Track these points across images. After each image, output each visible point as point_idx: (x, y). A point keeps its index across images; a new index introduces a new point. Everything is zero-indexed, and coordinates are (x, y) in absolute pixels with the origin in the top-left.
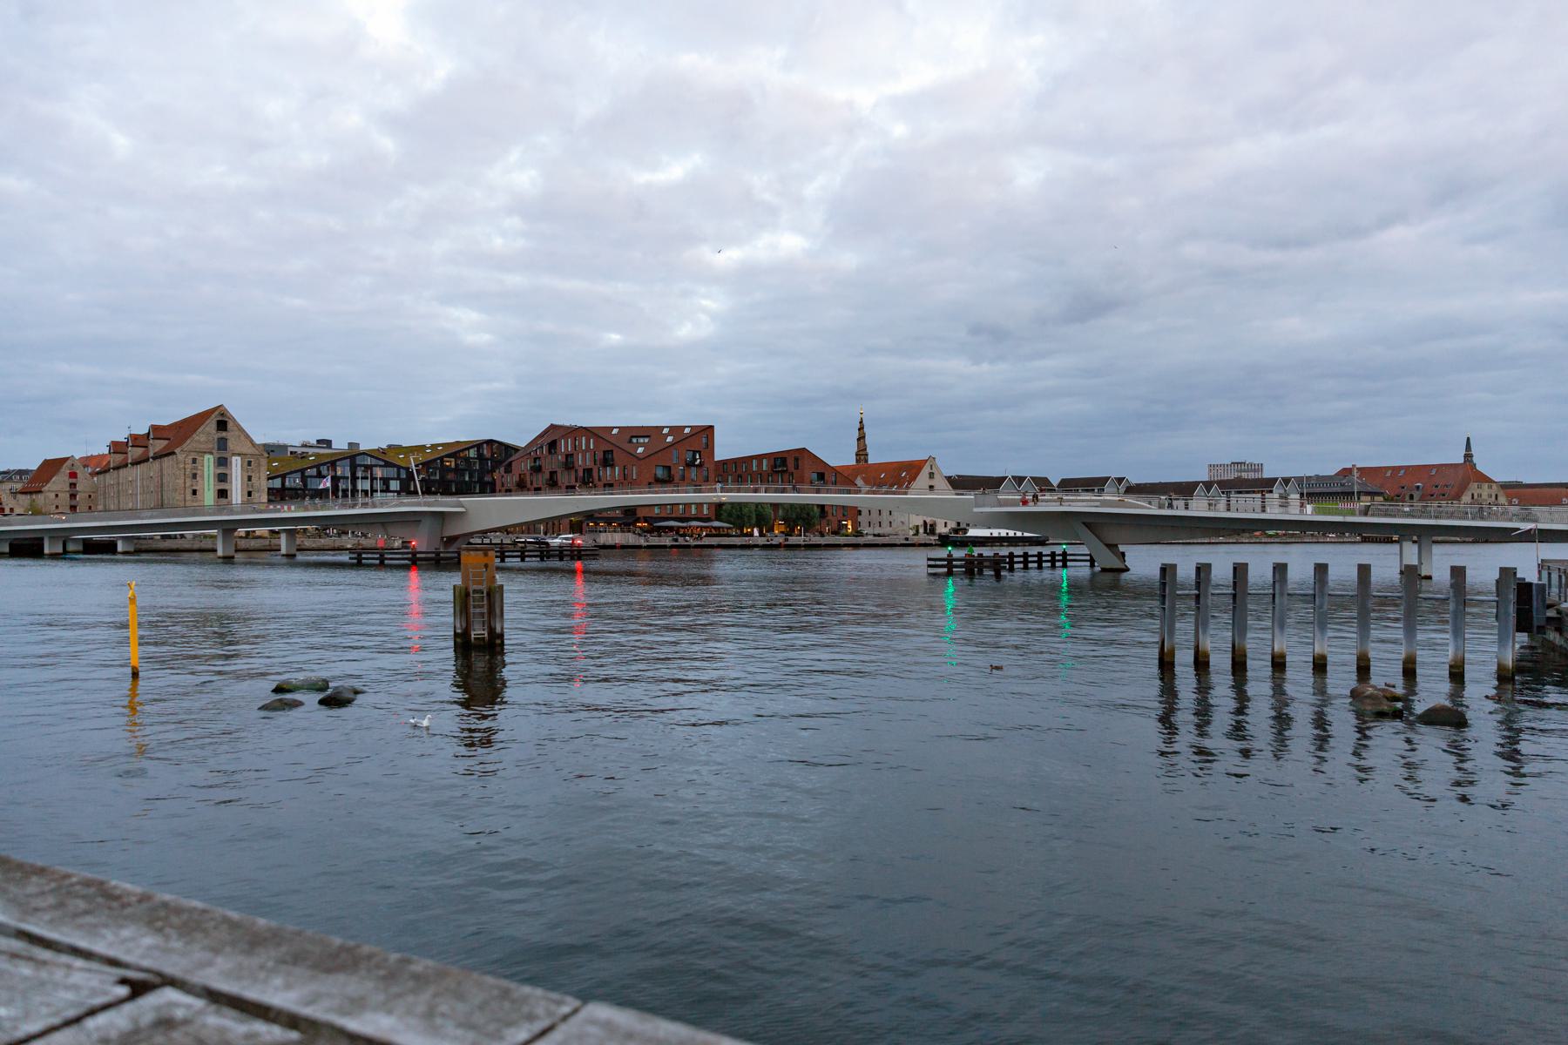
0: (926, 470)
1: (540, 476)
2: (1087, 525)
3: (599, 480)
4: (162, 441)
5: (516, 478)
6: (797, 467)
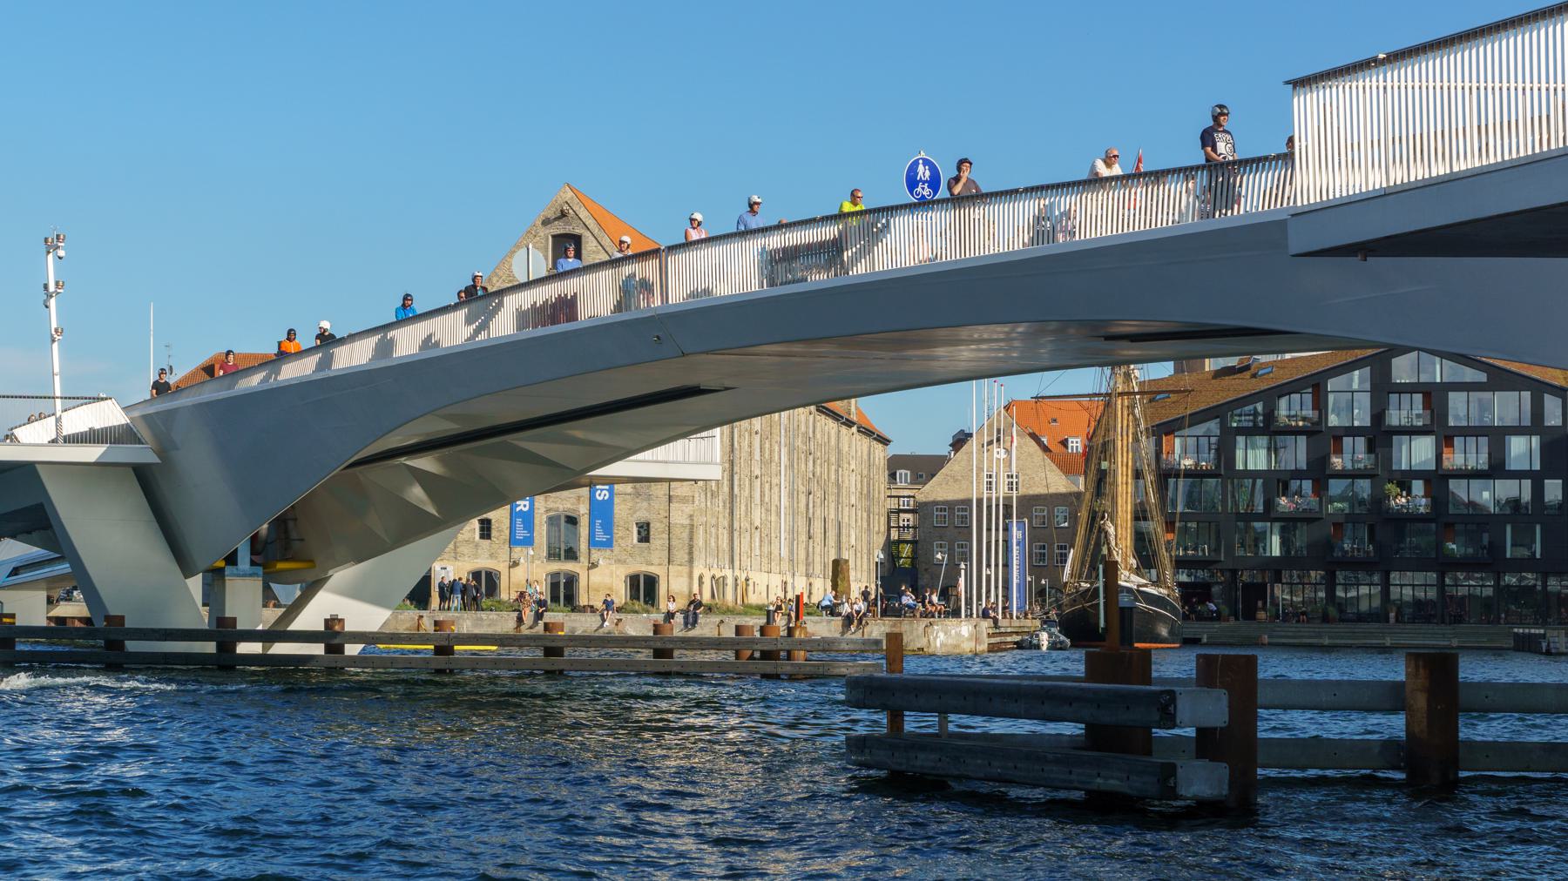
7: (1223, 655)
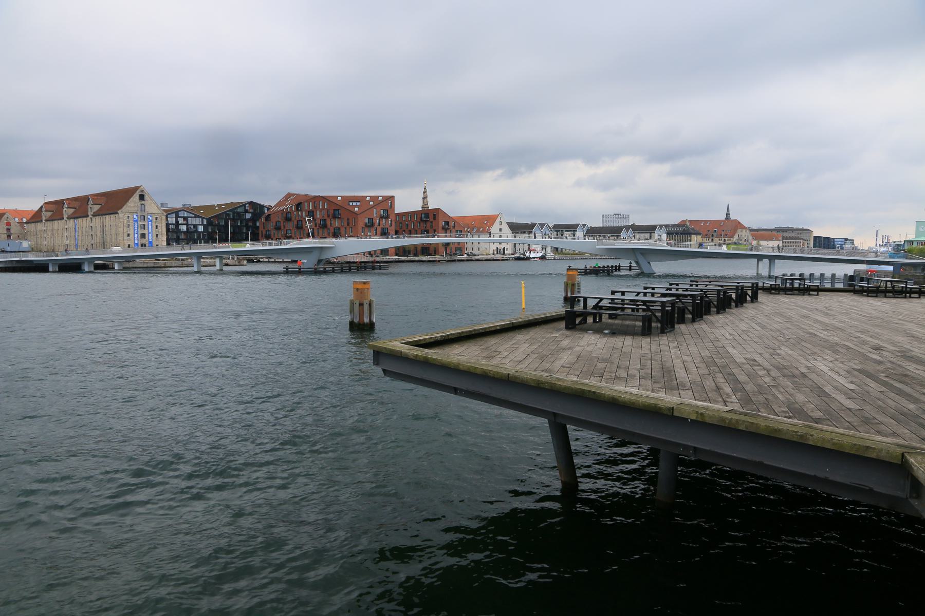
0: (498, 220)
1: (290, 223)
2: (642, 254)
3: (331, 226)
4: (98, 206)
5: (273, 224)
6: (435, 218)
7: (259, 233)
